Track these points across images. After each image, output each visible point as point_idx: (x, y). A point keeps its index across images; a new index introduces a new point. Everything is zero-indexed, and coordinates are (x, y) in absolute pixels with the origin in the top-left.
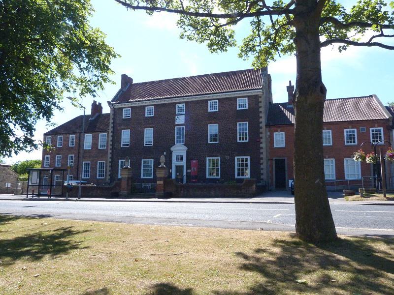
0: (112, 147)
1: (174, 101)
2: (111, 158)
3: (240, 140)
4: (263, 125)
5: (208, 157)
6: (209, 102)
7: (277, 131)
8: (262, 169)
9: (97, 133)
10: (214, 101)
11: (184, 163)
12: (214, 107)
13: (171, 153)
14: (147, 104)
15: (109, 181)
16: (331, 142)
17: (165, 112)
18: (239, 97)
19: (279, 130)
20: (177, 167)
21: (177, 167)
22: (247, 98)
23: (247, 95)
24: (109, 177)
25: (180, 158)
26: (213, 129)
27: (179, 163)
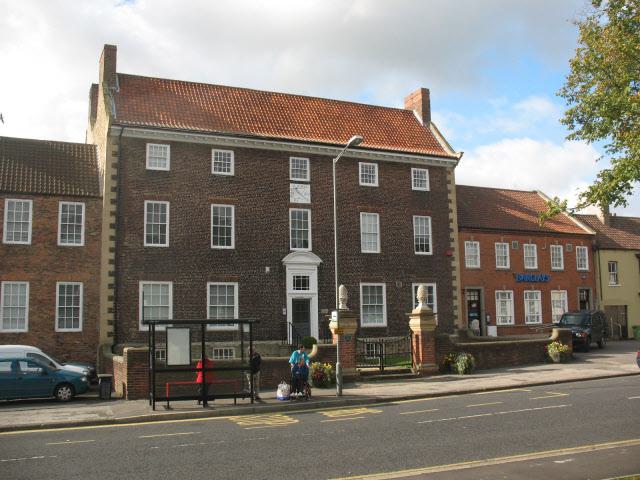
0: (117, 245)
1: (284, 147)
2: (115, 274)
3: (149, 241)
4: (454, 225)
5: (364, 281)
6: (213, 151)
7: (469, 239)
8: (456, 307)
9: (51, 199)
10: (368, 164)
11: (312, 292)
12: (367, 171)
13: (282, 270)
14: (150, 137)
15: (111, 340)
16: (508, 263)
17: (264, 170)
18: (152, 141)
19: (472, 237)
20: (295, 301)
21: (295, 301)
22: (168, 147)
23: (429, 164)
24: (111, 328)
25: (301, 283)
26: (370, 226)
27: (301, 294)
